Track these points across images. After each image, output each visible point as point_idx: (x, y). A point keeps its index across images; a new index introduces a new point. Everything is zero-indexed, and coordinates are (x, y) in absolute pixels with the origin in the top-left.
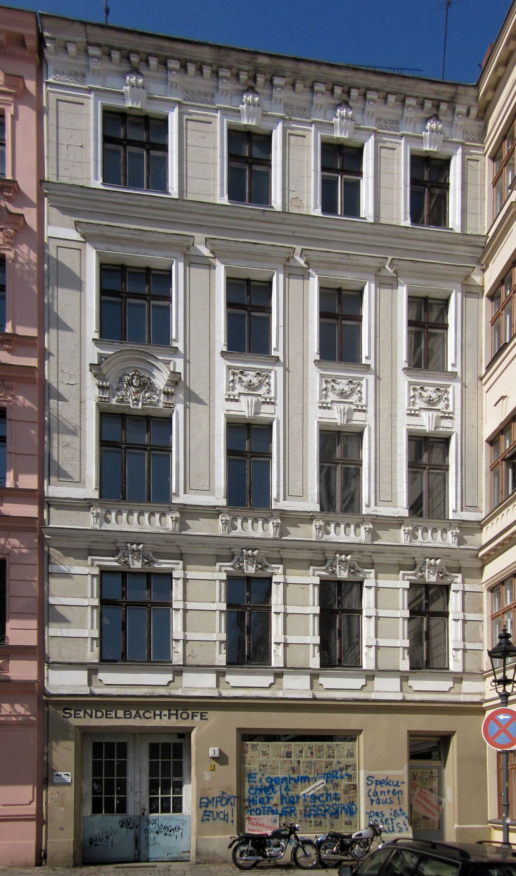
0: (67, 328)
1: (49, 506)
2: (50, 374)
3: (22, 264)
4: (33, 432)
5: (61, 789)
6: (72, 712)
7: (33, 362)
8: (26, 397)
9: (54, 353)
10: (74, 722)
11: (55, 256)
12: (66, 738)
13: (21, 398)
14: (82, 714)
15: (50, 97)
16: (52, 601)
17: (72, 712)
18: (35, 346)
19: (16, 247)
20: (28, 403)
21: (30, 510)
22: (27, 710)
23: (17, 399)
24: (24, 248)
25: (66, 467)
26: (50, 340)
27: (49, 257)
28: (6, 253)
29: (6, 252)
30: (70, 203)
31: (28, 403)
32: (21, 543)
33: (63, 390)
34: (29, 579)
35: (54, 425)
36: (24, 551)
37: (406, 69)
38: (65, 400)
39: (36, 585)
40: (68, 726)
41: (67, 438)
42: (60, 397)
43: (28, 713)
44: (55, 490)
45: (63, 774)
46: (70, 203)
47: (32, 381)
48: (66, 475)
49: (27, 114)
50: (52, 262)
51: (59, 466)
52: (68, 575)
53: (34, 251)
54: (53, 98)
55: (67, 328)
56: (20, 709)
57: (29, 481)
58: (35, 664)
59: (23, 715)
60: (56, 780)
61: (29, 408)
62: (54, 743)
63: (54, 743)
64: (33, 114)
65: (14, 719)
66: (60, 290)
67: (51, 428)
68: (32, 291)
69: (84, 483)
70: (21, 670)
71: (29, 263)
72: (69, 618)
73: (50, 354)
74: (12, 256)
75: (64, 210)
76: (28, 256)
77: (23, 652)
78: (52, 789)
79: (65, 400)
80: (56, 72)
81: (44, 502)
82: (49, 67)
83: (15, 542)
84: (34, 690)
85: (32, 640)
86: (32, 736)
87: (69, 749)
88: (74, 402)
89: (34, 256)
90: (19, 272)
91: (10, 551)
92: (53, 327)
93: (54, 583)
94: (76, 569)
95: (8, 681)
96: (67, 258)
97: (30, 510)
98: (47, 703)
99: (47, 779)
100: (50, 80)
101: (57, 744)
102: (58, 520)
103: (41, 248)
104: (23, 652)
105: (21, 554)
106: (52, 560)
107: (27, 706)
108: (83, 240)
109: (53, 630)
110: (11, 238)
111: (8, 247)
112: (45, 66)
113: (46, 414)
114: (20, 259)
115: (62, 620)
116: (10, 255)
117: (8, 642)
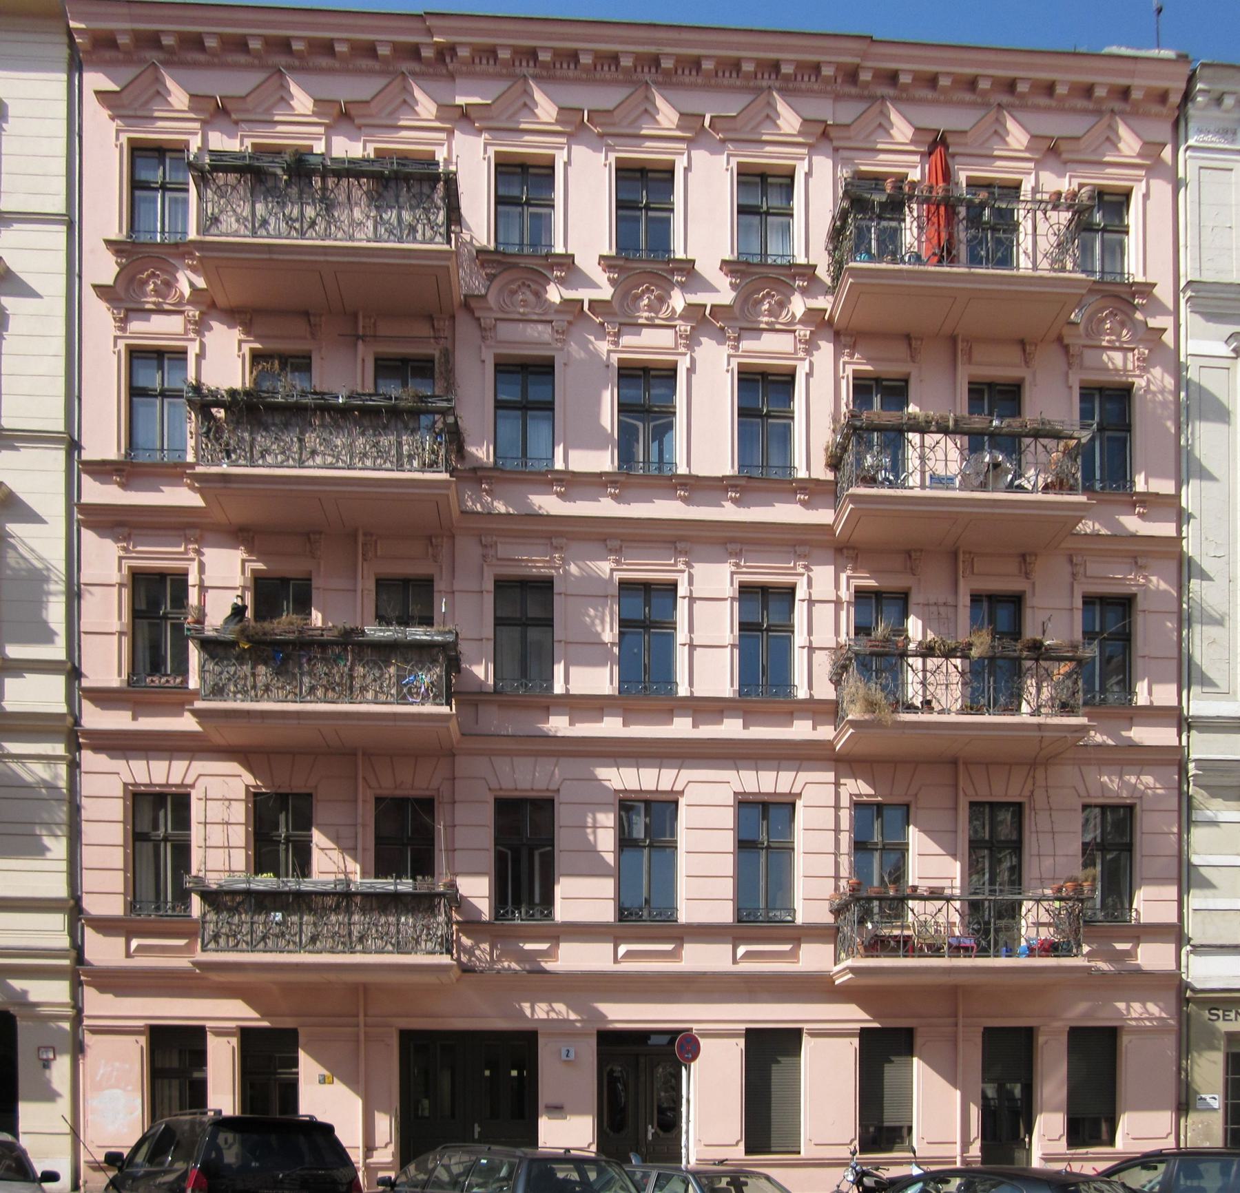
0: (1212, 478)
1: (1189, 729)
2: (1190, 547)
3: (1154, 393)
4: (1169, 624)
5: (1205, 1116)
6: (1220, 1013)
7: (1166, 529)
8: (1161, 577)
9: (1196, 514)
10: (1223, 1026)
11: (1196, 379)
12: (1212, 1047)
13: (1154, 579)
14: (1233, 1015)
15: (1187, 164)
16: (1195, 860)
17: (1220, 1013)
18: (1171, 507)
19: (1148, 372)
20: (1163, 586)
21: (1164, 736)
22: (1162, 1009)
23: (1150, 581)
24: (1157, 372)
25: (1211, 673)
26: (1189, 497)
27: (1188, 381)
28: (1136, 380)
29: (1134, 379)
30: (1218, 307)
31: (1163, 586)
32: (1156, 780)
33: (1207, 565)
34: (1166, 830)
35: (1196, 614)
36: (1159, 791)
37: (1017, 764)
38: (1210, 579)
39: (1174, 838)
40: (1213, 1032)
41: (1211, 631)
42: (1204, 576)
43: (1164, 1015)
44: (1199, 705)
45: (1207, 1097)
46: (1218, 307)
47: (1165, 555)
48: (1211, 683)
49: (1162, 189)
50: (1192, 388)
51: (1202, 672)
52: (1214, 823)
53: (1168, 372)
54: (1193, 166)
55: (1212, 478)
56: (1153, 1009)
57: (1165, 695)
58: (1171, 947)
59: (1156, 1018)
60: (1199, 1105)
61: (1165, 591)
62: (1195, 1054)
63: (1195, 1054)
64: (1168, 188)
65: (1148, 1024)
66: (1203, 424)
67: (1194, 619)
68: (1168, 429)
69: (1235, 693)
70: (1153, 956)
71: (1162, 391)
72: (1215, 882)
73: (1190, 516)
74: (1144, 384)
75: (1210, 317)
76: (1162, 381)
77: (1156, 932)
78: (1193, 1117)
79: (1210, 579)
80: (1200, 131)
81: (1184, 723)
82: (1190, 125)
83: (1148, 780)
84: (1175, 988)
85: (1168, 915)
86: (1169, 1045)
87: (1215, 1062)
88: (1220, 581)
89: (1169, 382)
90: (1150, 405)
91: (1143, 792)
92: (1195, 477)
93: (1198, 835)
94: (1224, 816)
95: (1139, 972)
96: (1210, 381)
97: (1164, 736)
98: (1188, 1000)
99: (1187, 1104)
100: (1191, 142)
101: (1200, 1055)
102: (1202, 747)
103: (1178, 369)
104: (1156, 932)
105: (1155, 795)
106: (1195, 803)
107: (1161, 1004)
108: (1233, 355)
109: (1196, 900)
110: (1144, 360)
111: (1137, 372)
112: (1182, 124)
113: (1185, 599)
114: (1152, 387)
115: (1207, 884)
116: (1140, 383)
117: (1137, 919)
